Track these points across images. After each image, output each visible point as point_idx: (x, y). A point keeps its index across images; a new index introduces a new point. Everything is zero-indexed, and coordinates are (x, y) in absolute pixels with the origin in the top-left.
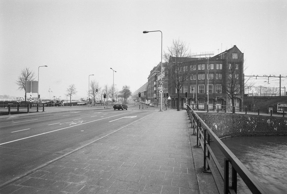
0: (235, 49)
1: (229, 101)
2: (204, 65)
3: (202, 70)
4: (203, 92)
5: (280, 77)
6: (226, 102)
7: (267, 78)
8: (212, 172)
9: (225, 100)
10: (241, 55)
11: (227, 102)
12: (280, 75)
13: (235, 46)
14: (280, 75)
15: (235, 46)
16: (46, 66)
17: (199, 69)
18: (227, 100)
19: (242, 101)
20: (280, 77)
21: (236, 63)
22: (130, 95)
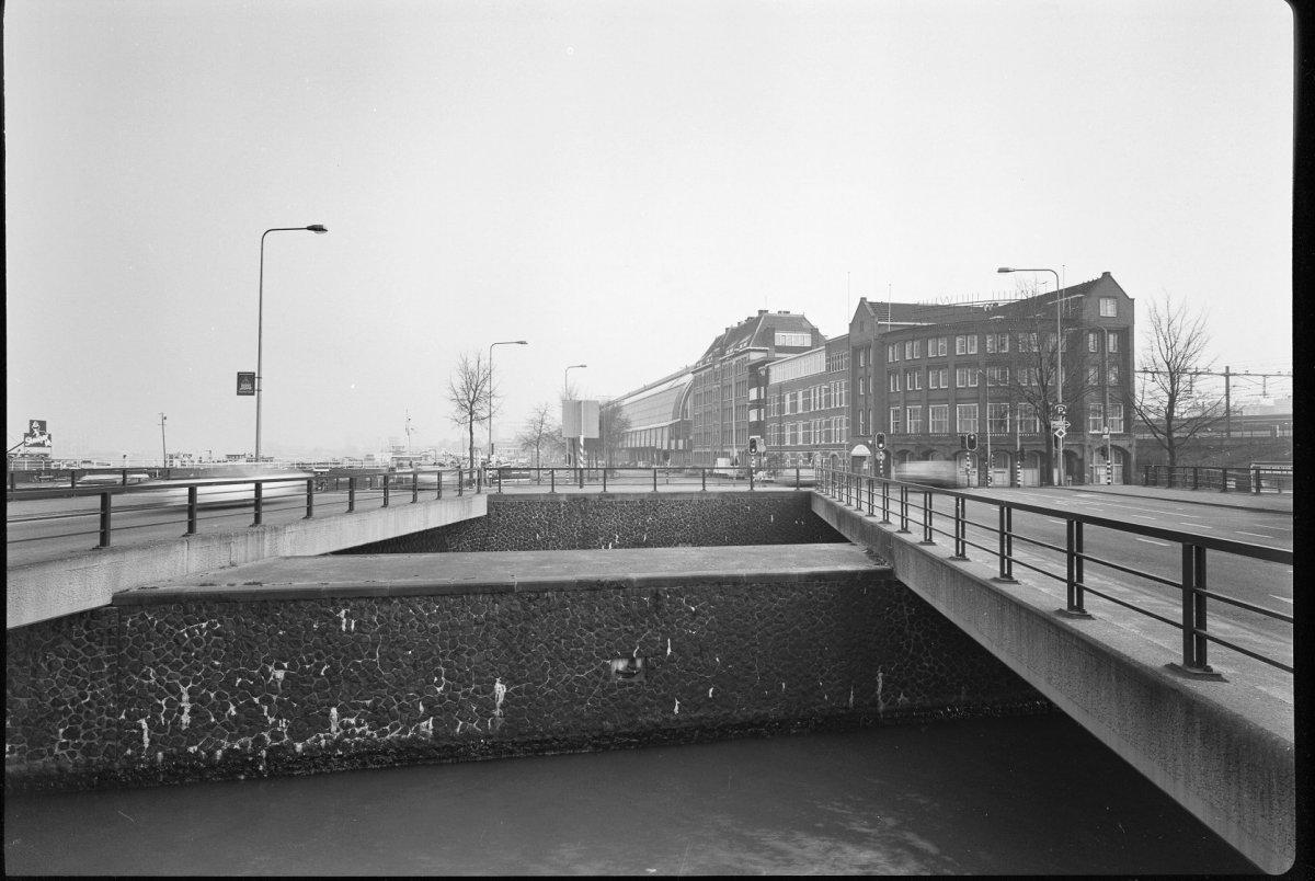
0: (1105, 285)
1: (1092, 459)
2: (976, 337)
3: (938, 357)
4: (1035, 430)
5: (1227, 375)
6: (1082, 460)
7: (1261, 379)
8: (263, 375)
9: (1080, 456)
10: (1126, 304)
11: (1087, 460)
12: (1227, 368)
13: (1106, 275)
14: (1227, 368)
15: (1106, 275)
16: (522, 343)
17: (930, 355)
18: (1087, 454)
19: (1134, 458)
20: (1227, 375)
21: (1110, 331)
22: (618, 409)
